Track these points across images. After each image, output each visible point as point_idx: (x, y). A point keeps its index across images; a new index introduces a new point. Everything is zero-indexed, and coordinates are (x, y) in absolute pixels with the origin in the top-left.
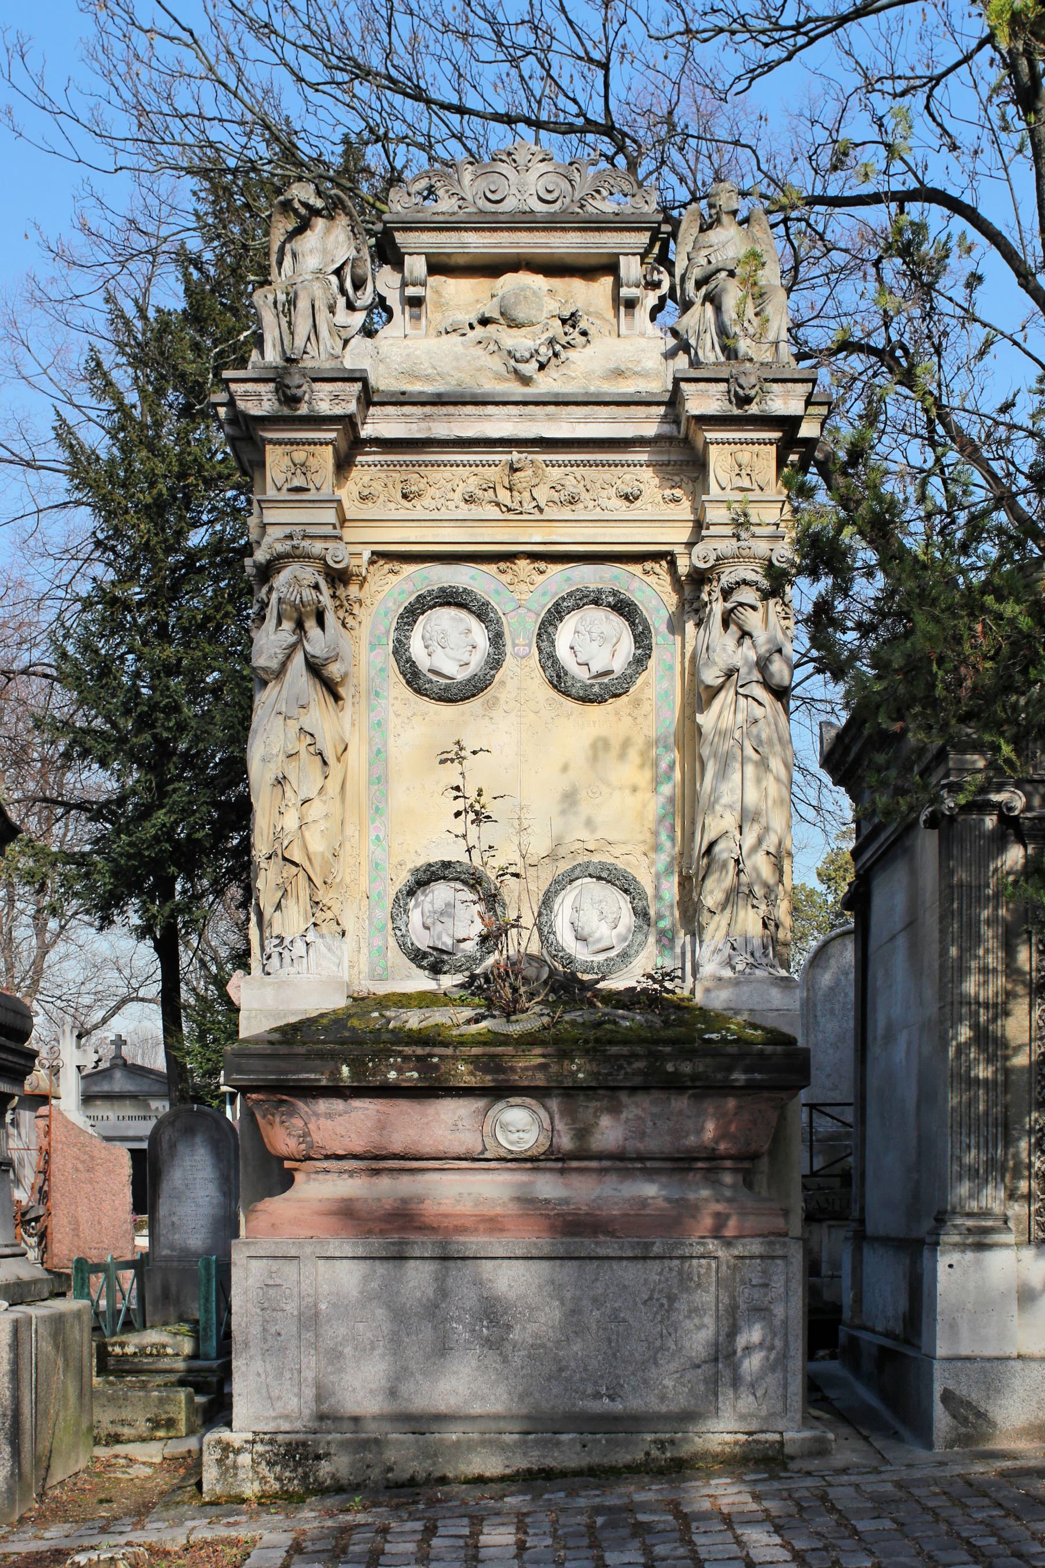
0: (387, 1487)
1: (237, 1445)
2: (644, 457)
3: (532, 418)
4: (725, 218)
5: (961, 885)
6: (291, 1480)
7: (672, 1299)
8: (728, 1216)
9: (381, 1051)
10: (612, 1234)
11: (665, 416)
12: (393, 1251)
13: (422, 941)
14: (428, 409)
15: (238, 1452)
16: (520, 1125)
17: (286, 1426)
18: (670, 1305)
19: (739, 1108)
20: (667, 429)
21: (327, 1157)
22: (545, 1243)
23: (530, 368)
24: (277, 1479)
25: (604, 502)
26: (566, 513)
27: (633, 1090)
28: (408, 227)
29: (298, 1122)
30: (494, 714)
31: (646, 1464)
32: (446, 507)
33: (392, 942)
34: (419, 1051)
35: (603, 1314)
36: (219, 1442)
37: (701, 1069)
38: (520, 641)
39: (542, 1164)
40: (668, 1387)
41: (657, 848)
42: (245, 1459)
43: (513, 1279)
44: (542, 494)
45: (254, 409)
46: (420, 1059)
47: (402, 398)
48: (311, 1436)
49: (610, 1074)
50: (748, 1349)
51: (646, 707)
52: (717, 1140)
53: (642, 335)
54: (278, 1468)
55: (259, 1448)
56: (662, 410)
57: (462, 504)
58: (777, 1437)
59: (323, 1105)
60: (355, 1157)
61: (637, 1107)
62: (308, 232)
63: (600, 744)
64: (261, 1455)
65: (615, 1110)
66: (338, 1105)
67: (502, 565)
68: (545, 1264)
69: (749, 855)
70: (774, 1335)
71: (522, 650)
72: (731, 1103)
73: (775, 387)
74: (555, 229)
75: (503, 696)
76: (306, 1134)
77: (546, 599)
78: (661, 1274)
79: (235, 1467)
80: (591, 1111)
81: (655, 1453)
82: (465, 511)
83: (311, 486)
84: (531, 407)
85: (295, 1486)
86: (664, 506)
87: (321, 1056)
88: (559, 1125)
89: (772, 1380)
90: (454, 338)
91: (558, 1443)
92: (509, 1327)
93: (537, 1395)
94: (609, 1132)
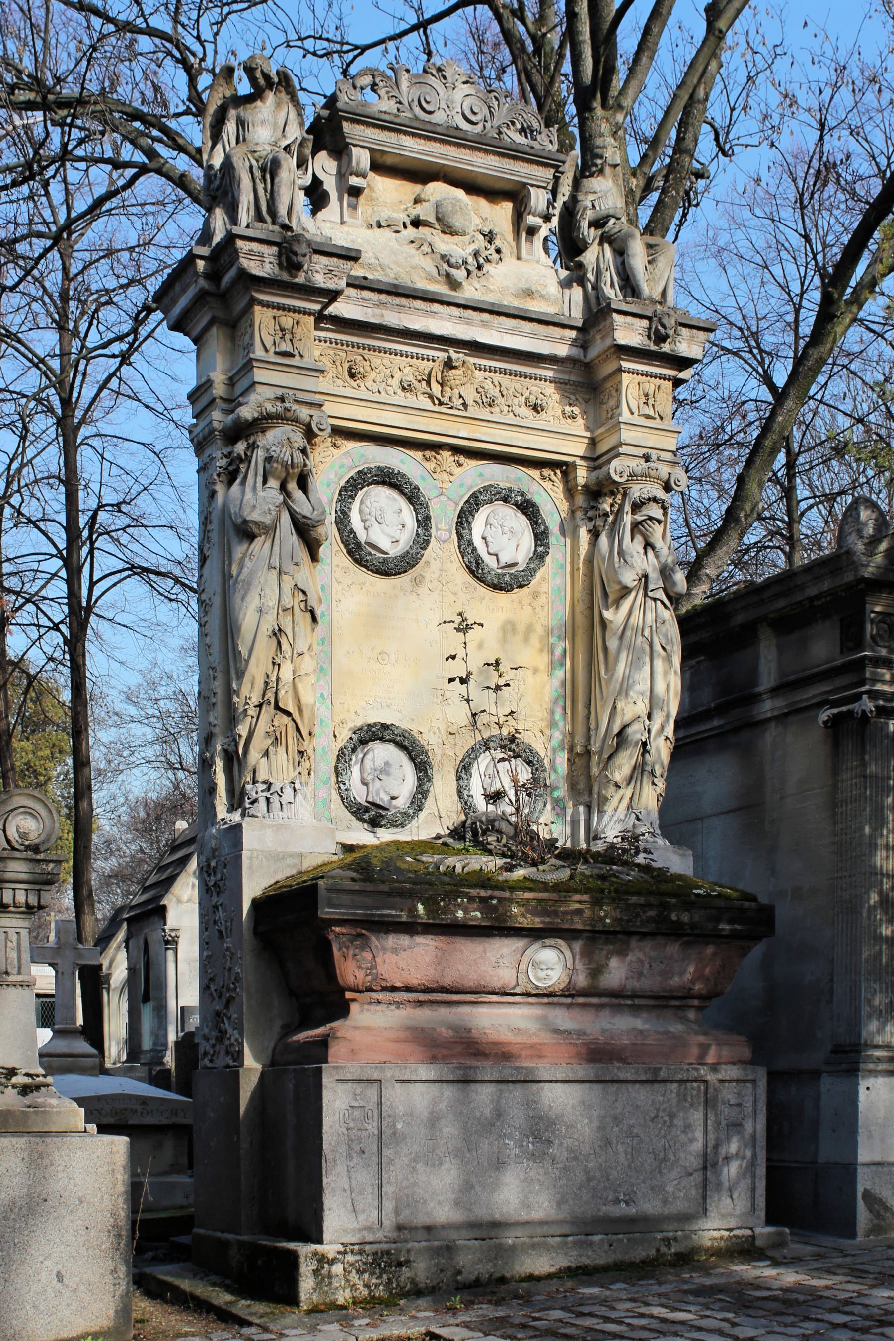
0: (457, 1289)
1: (331, 1256)
2: (550, 374)
3: (469, 322)
4: (608, 170)
5: (871, 777)
6: (377, 1286)
7: (672, 1116)
8: (708, 1046)
9: (451, 891)
10: (624, 1061)
11: (575, 340)
12: (459, 1075)
13: (359, 794)
14: (384, 297)
15: (331, 1262)
16: (551, 964)
17: (370, 1237)
18: (671, 1122)
19: (714, 954)
20: (576, 352)
21: (385, 989)
22: (582, 1071)
23: (459, 274)
24: (366, 1286)
25: (517, 410)
26: (484, 413)
27: (644, 935)
28: (359, 119)
29: (368, 955)
30: (420, 591)
31: (655, 1259)
32: (384, 392)
33: (335, 796)
34: (483, 893)
35: (621, 1130)
36: (315, 1253)
37: (696, 919)
38: (442, 526)
39: (555, 999)
40: (678, 1192)
41: (552, 724)
42: (338, 1269)
43: (563, 1098)
44: (470, 396)
45: (255, 268)
46: (483, 900)
47: (364, 283)
48: (394, 1246)
49: (629, 921)
50: (727, 1159)
51: (543, 599)
52: (693, 982)
53: (538, 262)
54: (366, 1276)
55: (350, 1258)
56: (573, 334)
57: (399, 391)
58: (749, 1232)
59: (392, 940)
60: (408, 989)
61: (640, 952)
62: (259, 103)
63: (509, 627)
64: (351, 1265)
65: (622, 953)
66: (404, 940)
67: (428, 454)
68: (577, 1086)
69: (655, 738)
70: (746, 1146)
71: (444, 535)
72: (710, 950)
73: (684, 331)
74: (480, 150)
75: (428, 575)
76: (374, 967)
77: (462, 491)
78: (663, 1095)
79: (330, 1276)
80: (604, 952)
81: (663, 1249)
82: (401, 398)
83: (296, 352)
84: (470, 312)
85: (380, 1292)
86: (563, 421)
87: (402, 893)
88: (579, 966)
89: (745, 1183)
90: (387, 233)
91: (591, 1243)
92: (550, 1142)
93: (571, 1202)
94: (617, 972)
